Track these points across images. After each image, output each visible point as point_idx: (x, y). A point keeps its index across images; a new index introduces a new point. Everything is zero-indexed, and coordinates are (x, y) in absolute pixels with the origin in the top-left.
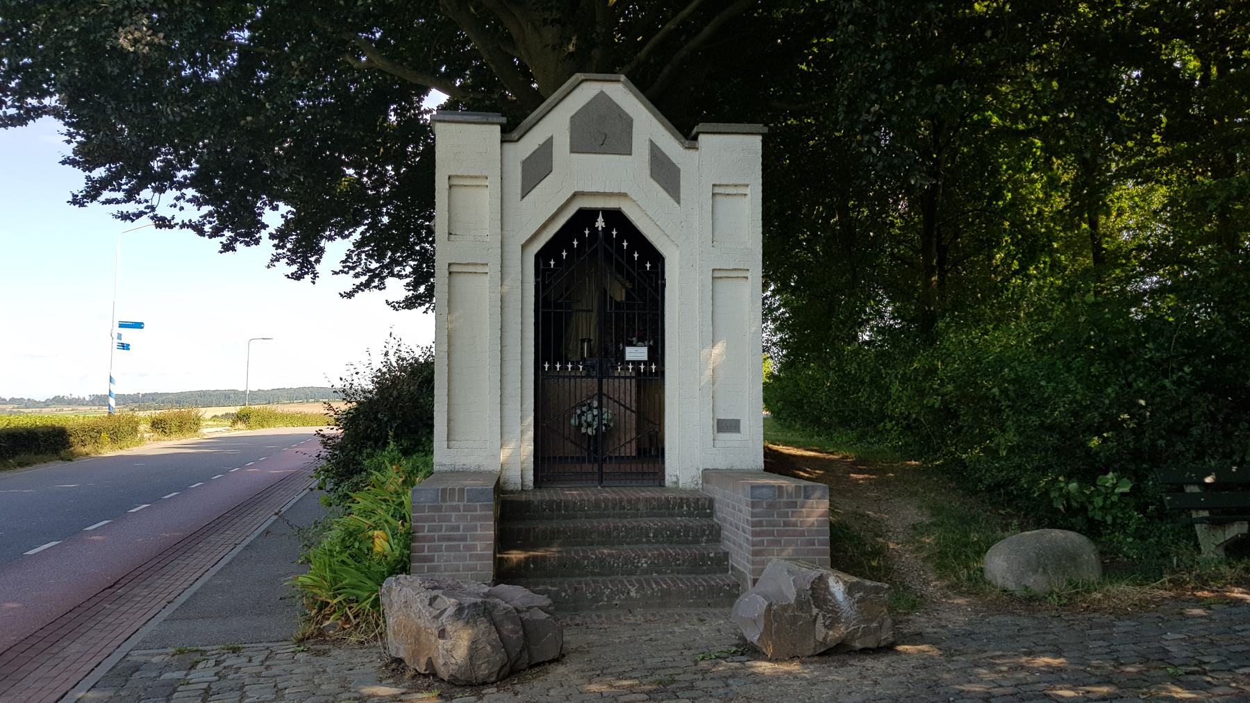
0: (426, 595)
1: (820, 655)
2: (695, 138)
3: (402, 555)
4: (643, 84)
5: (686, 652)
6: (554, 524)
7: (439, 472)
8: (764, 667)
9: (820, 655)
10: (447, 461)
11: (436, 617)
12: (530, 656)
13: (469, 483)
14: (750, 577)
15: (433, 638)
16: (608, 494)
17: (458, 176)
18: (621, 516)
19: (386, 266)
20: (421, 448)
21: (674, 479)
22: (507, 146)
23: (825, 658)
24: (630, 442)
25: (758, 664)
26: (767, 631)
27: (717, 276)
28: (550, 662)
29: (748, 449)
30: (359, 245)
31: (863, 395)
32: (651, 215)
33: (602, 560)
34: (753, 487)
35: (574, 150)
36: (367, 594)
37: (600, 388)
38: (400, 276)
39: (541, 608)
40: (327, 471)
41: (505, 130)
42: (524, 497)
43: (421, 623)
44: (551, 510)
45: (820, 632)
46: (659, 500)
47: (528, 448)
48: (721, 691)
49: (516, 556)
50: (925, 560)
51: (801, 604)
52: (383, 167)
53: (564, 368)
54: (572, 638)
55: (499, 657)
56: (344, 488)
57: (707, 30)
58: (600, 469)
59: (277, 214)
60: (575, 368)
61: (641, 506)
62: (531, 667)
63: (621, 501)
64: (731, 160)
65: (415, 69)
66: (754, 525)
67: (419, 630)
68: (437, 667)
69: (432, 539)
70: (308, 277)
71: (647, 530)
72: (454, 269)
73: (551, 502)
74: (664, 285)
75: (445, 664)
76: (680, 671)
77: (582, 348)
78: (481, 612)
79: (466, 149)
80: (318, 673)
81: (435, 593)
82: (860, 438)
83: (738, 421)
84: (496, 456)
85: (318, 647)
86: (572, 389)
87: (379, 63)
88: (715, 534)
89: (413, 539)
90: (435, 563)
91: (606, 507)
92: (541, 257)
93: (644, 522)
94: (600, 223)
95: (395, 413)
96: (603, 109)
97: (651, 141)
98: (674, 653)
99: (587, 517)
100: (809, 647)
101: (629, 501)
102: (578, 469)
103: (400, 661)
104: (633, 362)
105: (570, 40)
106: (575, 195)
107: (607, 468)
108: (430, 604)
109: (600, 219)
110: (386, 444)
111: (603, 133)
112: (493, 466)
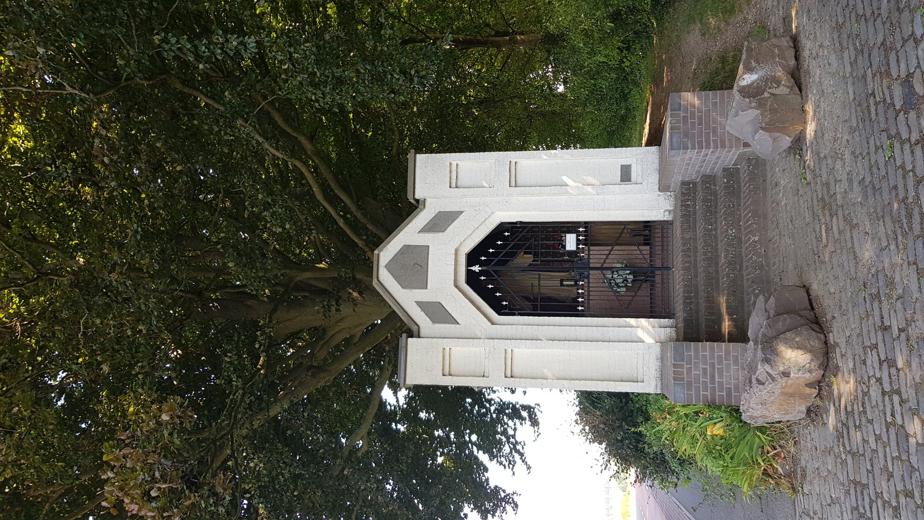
0: (756, 388)
1: (800, 90)
2: (418, 201)
3: (725, 412)
4: (377, 242)
5: (801, 192)
6: (702, 301)
7: (662, 389)
8: (810, 129)
9: (800, 90)
10: (653, 383)
11: (773, 379)
12: (805, 309)
13: (670, 361)
14: (742, 150)
15: (790, 382)
16: (678, 261)
18: (696, 251)
19: (508, 438)
20: (644, 408)
21: (667, 213)
22: (422, 334)
23: (803, 87)
24: (641, 251)
25: (808, 136)
26: (784, 131)
27: (514, 183)
28: (809, 295)
29: (641, 158)
30: (492, 457)
31: (604, 84)
32: (471, 232)
33: (730, 263)
34: (672, 148)
35: (425, 287)
36: (757, 439)
37: (597, 269)
38: (515, 430)
39: (766, 302)
40: (662, 480)
41: (411, 335)
42: (681, 325)
43: (778, 392)
44: (691, 303)
45: (782, 90)
46: (682, 222)
48: (829, 161)
49: (726, 325)
50: (727, 24)
51: (761, 105)
52: (436, 438)
53: (582, 295)
54: (791, 279)
55: (805, 331)
56: (674, 465)
57: (344, 197)
58: (659, 269)
59: (470, 515)
60: (582, 287)
61: (687, 236)
62: (813, 309)
63: (683, 251)
64: (435, 176)
65: (368, 406)
66: (701, 147)
67: (783, 394)
68: (813, 380)
69: (713, 389)
70: (516, 498)
71: (706, 230)
72: (509, 374)
73: (685, 303)
74: (521, 222)
75: (810, 371)
76: (815, 195)
77: (568, 285)
78: (769, 353)
79: (426, 362)
80: (819, 474)
81: (754, 381)
82: (636, 84)
83: (622, 166)
84: (650, 346)
85: (799, 476)
86: (598, 293)
87: (364, 430)
88: (709, 180)
89: (714, 403)
90: (732, 387)
91: (689, 262)
92: (500, 311)
93: (700, 231)
94: (476, 268)
95: (618, 421)
96: (400, 267)
98: (802, 201)
99: (696, 276)
100: (795, 98)
101: (684, 245)
102: (660, 285)
103: (809, 411)
104: (578, 245)
105: (350, 293)
106: (456, 286)
107: (658, 263)
108: (763, 384)
109: (473, 268)
110: (640, 434)
111: (414, 266)
112: (657, 349)
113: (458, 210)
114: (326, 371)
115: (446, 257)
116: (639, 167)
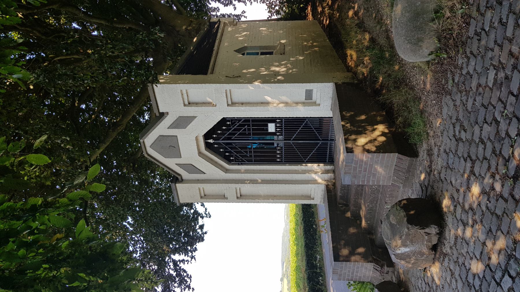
17: (200, 195)
44: (345, 189)
47: (315, 166)
64: (170, 95)
83: (306, 90)
94: (211, 141)
97: (168, 128)
104: (276, 129)
109: (209, 141)
111: (170, 146)
113: (192, 115)
114: (120, 125)
115: (190, 145)
116: (319, 94)
